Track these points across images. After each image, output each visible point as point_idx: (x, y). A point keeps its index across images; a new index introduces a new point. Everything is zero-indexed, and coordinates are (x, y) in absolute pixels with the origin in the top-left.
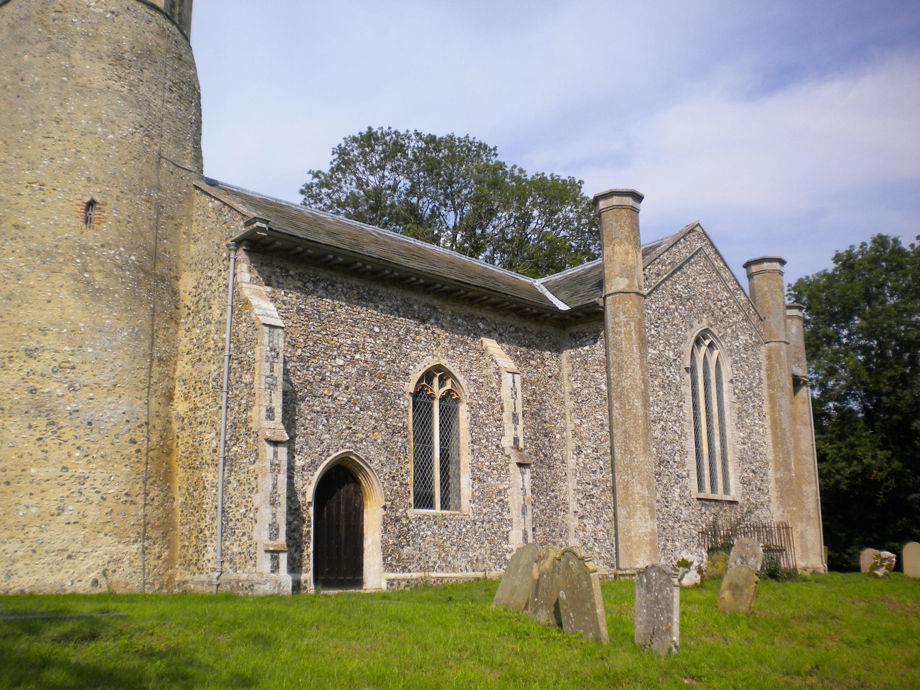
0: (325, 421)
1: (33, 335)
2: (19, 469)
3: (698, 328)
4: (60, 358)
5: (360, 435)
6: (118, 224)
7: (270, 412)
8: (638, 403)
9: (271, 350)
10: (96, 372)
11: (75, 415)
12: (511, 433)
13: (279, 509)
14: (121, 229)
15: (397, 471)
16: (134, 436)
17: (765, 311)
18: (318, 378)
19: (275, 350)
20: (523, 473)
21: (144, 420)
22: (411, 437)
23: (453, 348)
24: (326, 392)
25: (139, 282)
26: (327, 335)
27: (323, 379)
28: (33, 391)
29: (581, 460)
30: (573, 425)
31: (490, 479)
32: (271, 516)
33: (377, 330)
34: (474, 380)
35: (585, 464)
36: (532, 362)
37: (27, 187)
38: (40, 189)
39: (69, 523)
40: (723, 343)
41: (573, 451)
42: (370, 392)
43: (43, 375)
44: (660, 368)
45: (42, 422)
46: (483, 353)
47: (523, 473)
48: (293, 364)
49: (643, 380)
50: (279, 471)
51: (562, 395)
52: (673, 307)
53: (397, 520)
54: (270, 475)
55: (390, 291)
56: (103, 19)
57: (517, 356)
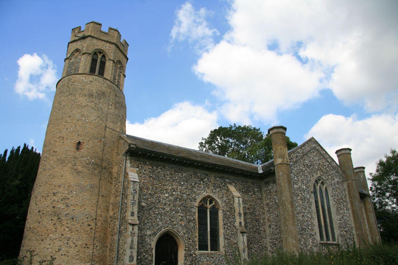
0: (160, 217)
1: (56, 188)
2: (47, 235)
3: (316, 176)
4: (64, 195)
5: (175, 223)
6: (88, 149)
7: (132, 214)
8: (289, 206)
9: (134, 190)
10: (76, 200)
11: (67, 215)
12: (239, 220)
13: (134, 250)
14: (89, 151)
15: (191, 236)
16: (90, 223)
17: (345, 169)
18: (157, 201)
19: (135, 190)
20: (243, 236)
21: (95, 217)
22: (197, 223)
23: (215, 189)
24: (161, 206)
25: (95, 169)
26: (162, 185)
27: (159, 202)
28: (54, 207)
29: (271, 230)
30: (268, 217)
31: (231, 239)
32: (130, 253)
33: (182, 183)
34: (224, 201)
35: (273, 232)
36: (250, 193)
37: (59, 139)
38: (63, 139)
39: (62, 255)
40: (328, 182)
41: (268, 227)
42: (179, 206)
43: (58, 202)
44: (300, 192)
45: (55, 218)
46: (228, 190)
47: (243, 236)
48: (147, 196)
49: (291, 197)
50: (134, 236)
51: (263, 206)
52: (304, 169)
53: (191, 255)
54: (130, 237)
55: (188, 169)
56: (87, 84)
57: (243, 191)
